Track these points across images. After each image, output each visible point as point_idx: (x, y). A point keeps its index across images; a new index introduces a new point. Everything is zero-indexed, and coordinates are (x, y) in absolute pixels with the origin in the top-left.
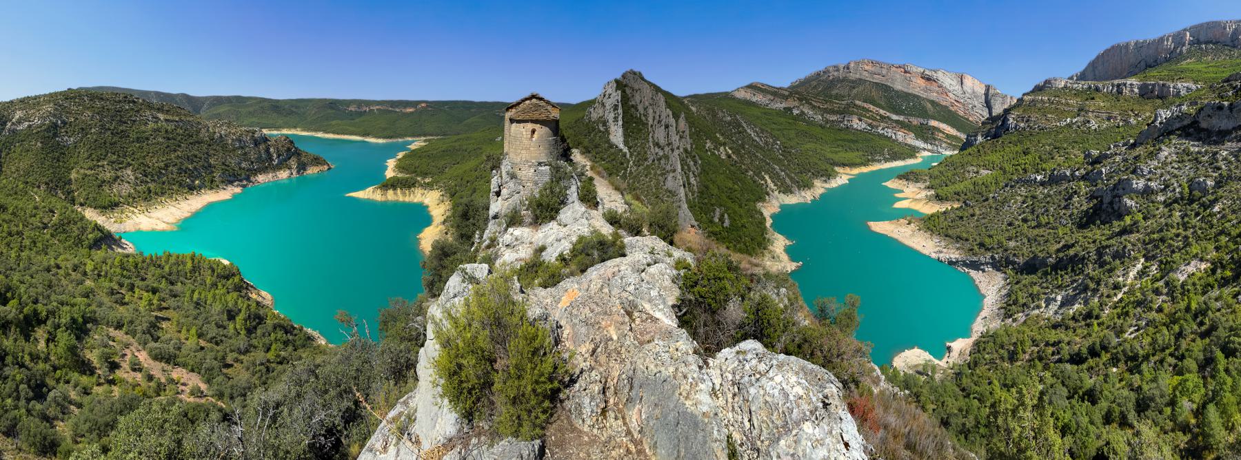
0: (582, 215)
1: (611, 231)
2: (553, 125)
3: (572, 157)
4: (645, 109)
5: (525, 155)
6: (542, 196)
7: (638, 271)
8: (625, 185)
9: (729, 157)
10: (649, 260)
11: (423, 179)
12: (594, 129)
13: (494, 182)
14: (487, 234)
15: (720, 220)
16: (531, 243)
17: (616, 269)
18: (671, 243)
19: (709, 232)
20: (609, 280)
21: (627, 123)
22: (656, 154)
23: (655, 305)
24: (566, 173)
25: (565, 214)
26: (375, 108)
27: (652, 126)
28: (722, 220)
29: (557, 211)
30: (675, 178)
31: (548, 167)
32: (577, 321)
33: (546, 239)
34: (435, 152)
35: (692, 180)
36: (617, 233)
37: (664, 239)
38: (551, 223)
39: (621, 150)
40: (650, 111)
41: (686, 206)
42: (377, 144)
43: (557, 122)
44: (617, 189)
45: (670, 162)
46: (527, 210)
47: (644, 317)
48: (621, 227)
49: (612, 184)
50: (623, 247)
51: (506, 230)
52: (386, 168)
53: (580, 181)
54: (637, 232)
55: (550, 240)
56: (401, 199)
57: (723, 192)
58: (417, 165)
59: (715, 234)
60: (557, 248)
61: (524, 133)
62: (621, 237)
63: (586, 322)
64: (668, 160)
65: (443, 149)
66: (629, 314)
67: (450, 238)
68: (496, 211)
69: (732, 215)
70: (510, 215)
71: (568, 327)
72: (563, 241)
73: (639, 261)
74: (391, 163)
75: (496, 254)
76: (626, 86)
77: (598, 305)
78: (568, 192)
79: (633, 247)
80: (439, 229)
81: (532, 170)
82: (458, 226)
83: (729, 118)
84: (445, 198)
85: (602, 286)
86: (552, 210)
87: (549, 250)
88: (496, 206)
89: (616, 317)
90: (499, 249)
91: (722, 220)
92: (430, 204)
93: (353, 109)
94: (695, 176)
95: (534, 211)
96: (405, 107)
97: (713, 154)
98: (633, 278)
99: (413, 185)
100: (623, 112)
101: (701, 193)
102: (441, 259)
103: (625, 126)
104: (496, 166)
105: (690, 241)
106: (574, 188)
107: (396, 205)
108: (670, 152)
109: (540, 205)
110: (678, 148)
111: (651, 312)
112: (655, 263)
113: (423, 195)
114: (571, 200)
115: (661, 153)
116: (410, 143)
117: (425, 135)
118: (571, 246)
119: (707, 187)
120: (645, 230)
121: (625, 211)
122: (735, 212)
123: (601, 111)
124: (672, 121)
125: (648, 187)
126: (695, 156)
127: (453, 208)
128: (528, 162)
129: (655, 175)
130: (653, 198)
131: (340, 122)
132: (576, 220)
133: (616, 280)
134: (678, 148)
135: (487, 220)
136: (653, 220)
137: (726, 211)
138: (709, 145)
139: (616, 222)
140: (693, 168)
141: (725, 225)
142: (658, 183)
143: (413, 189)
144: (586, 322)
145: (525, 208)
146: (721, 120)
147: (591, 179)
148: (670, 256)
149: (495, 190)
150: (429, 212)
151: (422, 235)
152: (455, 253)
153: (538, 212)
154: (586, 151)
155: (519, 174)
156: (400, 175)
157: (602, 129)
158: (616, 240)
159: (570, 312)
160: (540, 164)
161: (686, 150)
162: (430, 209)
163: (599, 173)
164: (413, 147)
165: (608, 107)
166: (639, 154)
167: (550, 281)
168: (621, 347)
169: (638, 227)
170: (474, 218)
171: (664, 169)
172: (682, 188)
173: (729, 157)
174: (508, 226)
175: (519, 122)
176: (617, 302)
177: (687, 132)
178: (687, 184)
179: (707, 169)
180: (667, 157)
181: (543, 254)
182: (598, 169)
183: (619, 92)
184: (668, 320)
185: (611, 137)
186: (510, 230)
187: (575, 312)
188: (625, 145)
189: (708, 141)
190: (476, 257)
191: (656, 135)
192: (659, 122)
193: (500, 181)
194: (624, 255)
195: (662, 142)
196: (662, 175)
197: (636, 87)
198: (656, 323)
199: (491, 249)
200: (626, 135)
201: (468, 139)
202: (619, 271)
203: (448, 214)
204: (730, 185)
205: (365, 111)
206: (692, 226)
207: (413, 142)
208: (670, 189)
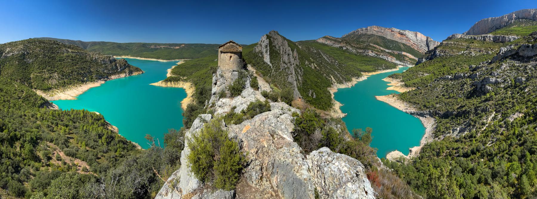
0: (252, 93)
1: (264, 100)
2: (239, 54)
4: (279, 47)
5: (227, 67)
6: (234, 85)
7: (276, 117)
8: (270, 80)
9: (316, 68)
10: (281, 112)
12: (257, 56)
13: (214, 79)
14: (211, 101)
15: (311, 95)
16: (230, 105)
18: (290, 105)
19: (307, 100)
20: (264, 121)
22: (284, 66)
23: (283, 132)
24: (245, 75)
25: (245, 93)
26: (162, 47)
27: (282, 54)
28: (312, 95)
29: (241, 91)
30: (292, 77)
31: (237, 72)
32: (249, 139)
34: (188, 66)
35: (300, 78)
37: (287, 103)
38: (238, 97)
39: (269, 65)
40: (281, 48)
41: (297, 89)
43: (241, 53)
44: (267, 82)
45: (290, 70)
46: (228, 91)
47: (279, 137)
48: (269, 98)
49: (265, 80)
50: (269, 107)
51: (219, 99)
52: (167, 73)
53: (251, 78)
54: (275, 100)
55: (238, 104)
56: (174, 86)
58: (180, 71)
59: (309, 101)
60: (241, 107)
61: (227, 58)
62: (269, 103)
63: (253, 139)
64: (289, 69)
65: (192, 64)
66: (272, 136)
67: (195, 103)
68: (215, 91)
69: (317, 93)
70: (220, 93)
71: (246, 142)
72: (243, 104)
74: (169, 71)
75: (215, 110)
76: (271, 37)
77: (259, 132)
78: (246, 83)
79: (274, 107)
80: (190, 99)
81: (230, 74)
83: (315, 51)
84: (193, 86)
86: (239, 91)
87: (238, 108)
88: (215, 89)
89: (266, 137)
90: (216, 108)
91: (312, 95)
92: (186, 88)
93: (153, 47)
94: (301, 76)
95: (231, 92)
96: (175, 46)
97: (309, 67)
98: (274, 120)
99: (179, 80)
100: (270, 49)
101: (303, 83)
102: (191, 112)
103: (271, 54)
104: (215, 72)
105: (299, 104)
106: (248, 81)
107: (172, 89)
108: (290, 66)
109: (233, 89)
110: (293, 64)
111: (282, 135)
112: (284, 114)
113: (183, 84)
114: (247, 86)
115: (286, 66)
116: (177, 62)
117: (184, 59)
119: (306, 81)
120: (279, 100)
121: (271, 91)
122: (318, 92)
124: (291, 52)
125: (280, 81)
126: (301, 68)
127: (196, 90)
128: (228, 70)
129: (283, 76)
131: (147, 53)
132: (249, 95)
133: (267, 121)
134: (293, 64)
135: (211, 95)
136: (282, 95)
137: (314, 91)
138: (307, 63)
139: (266, 96)
140: (300, 73)
141: (314, 97)
142: (285, 79)
143: (179, 82)
144: (253, 139)
145: (227, 90)
146: (312, 52)
147: (256, 77)
148: (290, 111)
149: (214, 82)
150: (186, 92)
151: (182, 102)
152: (197, 109)
153: (233, 92)
154: (253, 65)
155: (225, 75)
156: (173, 76)
157: (260, 56)
158: (267, 104)
159: (247, 135)
160: (234, 71)
161: (297, 65)
162: (186, 90)
163: (259, 75)
164: (179, 64)
165: (263, 46)
166: (276, 67)
167: (238, 122)
168: (269, 150)
170: (205, 94)
171: (287, 73)
173: (316, 68)
174: (220, 98)
175: (225, 53)
176: (267, 130)
177: (297, 57)
178: (297, 80)
179: (306, 73)
180: (288, 68)
181: (235, 110)
183: (268, 40)
184: (289, 139)
185: (264, 59)
186: (221, 99)
187: (249, 135)
188: (270, 63)
189: (306, 61)
190: (206, 111)
191: (284, 59)
192: (285, 53)
193: (216, 78)
194: (270, 110)
195: (287, 61)
196: (287, 76)
197: (275, 38)
199: (213, 108)
200: (271, 59)
202: (268, 117)
203: (194, 92)
204: (316, 80)
205: (158, 48)
206: (300, 98)
207: (179, 61)
208: (290, 82)
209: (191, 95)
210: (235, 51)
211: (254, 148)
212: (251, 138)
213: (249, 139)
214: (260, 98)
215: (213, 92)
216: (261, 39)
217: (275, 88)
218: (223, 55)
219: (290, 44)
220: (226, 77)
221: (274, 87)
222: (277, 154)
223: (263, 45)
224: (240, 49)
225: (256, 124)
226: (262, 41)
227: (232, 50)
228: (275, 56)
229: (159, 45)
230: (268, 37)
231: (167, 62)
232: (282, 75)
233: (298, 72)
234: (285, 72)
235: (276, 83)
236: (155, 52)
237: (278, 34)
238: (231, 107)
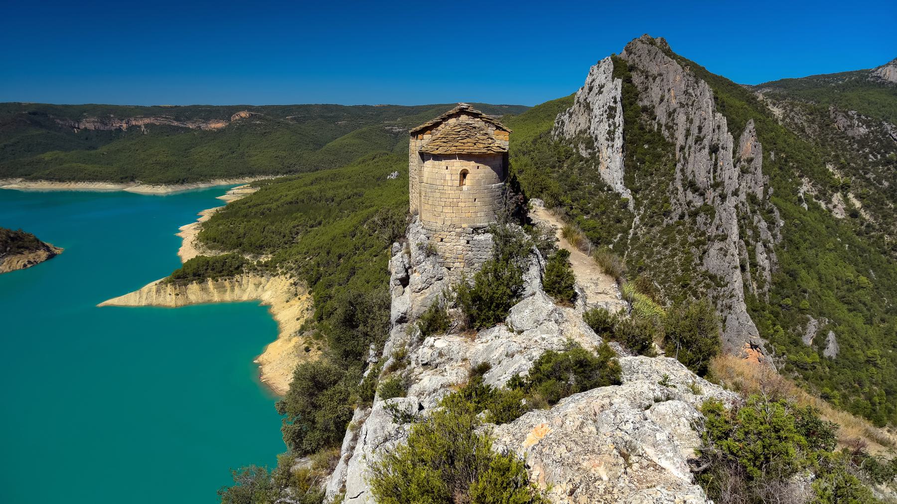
0: (549, 315)
1: (596, 344)
2: (499, 162)
3: (530, 215)
4: (670, 114)
5: (449, 215)
6: (480, 283)
7: (640, 407)
8: (622, 266)
9: (854, 214)
10: (658, 393)
11: (255, 257)
12: (569, 154)
13: (396, 265)
14: (389, 348)
15: (815, 342)
16: (464, 360)
17: (606, 401)
18: (703, 372)
19: (788, 362)
20: (595, 415)
21: (632, 142)
22: (689, 203)
23: (662, 451)
24: (521, 246)
25: (520, 314)
26: (140, 123)
27: (682, 148)
28: (820, 342)
29: (507, 308)
30: (724, 252)
31: (489, 236)
32: (549, 462)
33: (490, 353)
34: (274, 206)
35: (762, 258)
36: (606, 346)
37: (689, 364)
38: (497, 328)
39: (618, 195)
40: (681, 119)
41: (744, 307)
42: (154, 197)
43: (505, 156)
44: (609, 272)
45: (717, 221)
46: (455, 306)
47: (645, 463)
48: (613, 337)
49: (601, 263)
50: (617, 370)
51: (421, 340)
52: (179, 242)
53: (546, 258)
54: (642, 348)
55: (495, 355)
56: (216, 297)
57: (829, 288)
58: (242, 231)
59: (801, 367)
60: (508, 367)
61: (448, 177)
62: (613, 354)
63: (561, 462)
64: (713, 217)
65: (289, 199)
66: (626, 457)
67: (315, 356)
68: (403, 310)
69: (846, 336)
70: (427, 316)
71: (538, 468)
72: (517, 357)
73: (641, 393)
74: (189, 232)
75: (408, 377)
76: (632, 68)
77: (577, 443)
78: (524, 277)
79: (633, 371)
80: (293, 343)
81: (463, 241)
82: (338, 340)
83: (863, 130)
84: (300, 289)
85: (583, 423)
86: (498, 306)
87: (495, 370)
88: (399, 306)
89: (606, 457)
90: (412, 371)
91: (820, 342)
92: (273, 301)
93: (90, 126)
94: (768, 251)
95: (467, 309)
96: (207, 119)
97: (816, 208)
98: (632, 415)
99: (238, 270)
100: (626, 122)
101: (779, 285)
102: (311, 395)
103: (629, 149)
104: (399, 235)
105: (742, 374)
106: (534, 271)
107: (208, 310)
108: (718, 201)
109: (477, 298)
110: (735, 193)
111: (655, 459)
112: (668, 399)
113: (257, 285)
114: (529, 290)
115: (698, 202)
116: (223, 191)
117: (252, 174)
118: (530, 365)
119: (793, 275)
120: (656, 346)
121: (622, 312)
122: (854, 331)
123: (582, 120)
124: (727, 138)
125: (667, 266)
126: (771, 211)
127: (316, 306)
128: (454, 226)
129: (683, 244)
130: (676, 288)
131: (62, 155)
132: (538, 323)
133: (607, 415)
134: (735, 193)
135: (387, 326)
136: (671, 329)
137: (833, 326)
138: (806, 187)
139: (605, 330)
140: (765, 235)
141: (826, 353)
142: (688, 260)
143: (237, 277)
144: (561, 462)
145: (452, 304)
146: (843, 135)
147: (564, 254)
148: (696, 392)
149: (400, 276)
150: (272, 315)
151: (263, 358)
152: (335, 382)
153: (474, 310)
154: (554, 204)
155: (440, 247)
156: (209, 254)
157: (584, 154)
158: (607, 358)
159: (540, 449)
160: (476, 230)
161: (752, 198)
162: (274, 310)
163: (578, 244)
164: (229, 197)
165: (597, 112)
166: (652, 203)
167: (505, 415)
168: (613, 487)
169: (644, 340)
170: (365, 323)
171: (703, 233)
172: (738, 271)
173: (854, 214)
174: (425, 333)
175: (437, 157)
176: (609, 440)
177: (759, 161)
178: (749, 266)
179: (796, 237)
180: (710, 211)
181: (486, 376)
182: (576, 237)
183: (619, 82)
184: (684, 476)
185: (602, 169)
186: (429, 340)
187: (546, 451)
188: (626, 186)
189: (805, 180)
190: (373, 385)
191: (690, 167)
192: (699, 140)
193: (406, 261)
194: (619, 383)
195: (702, 179)
196: (698, 244)
197: (654, 70)
198: (661, 472)
199: (399, 372)
200: (630, 168)
201: (334, 178)
202: (611, 404)
203: (308, 315)
204: (849, 273)
205: (119, 129)
206: (754, 346)
207: (229, 188)
208: (712, 272)
209: (297, 326)
210: (480, 148)
211: (565, 483)
212: (553, 460)
213: (549, 462)
214: (581, 335)
215: (396, 312)
216: (589, 79)
217: (642, 298)
218: (434, 167)
219: (723, 96)
220: (447, 255)
221: (637, 295)
222: (638, 496)
223: (599, 104)
224: (501, 141)
225: (568, 422)
226: (591, 89)
227: (468, 147)
228: (647, 158)
229: (124, 113)
230: (622, 70)
231: (168, 198)
232: (674, 241)
233: (756, 230)
234: (692, 230)
235: (646, 274)
236: (103, 149)
237: (668, 53)
238: (469, 366)
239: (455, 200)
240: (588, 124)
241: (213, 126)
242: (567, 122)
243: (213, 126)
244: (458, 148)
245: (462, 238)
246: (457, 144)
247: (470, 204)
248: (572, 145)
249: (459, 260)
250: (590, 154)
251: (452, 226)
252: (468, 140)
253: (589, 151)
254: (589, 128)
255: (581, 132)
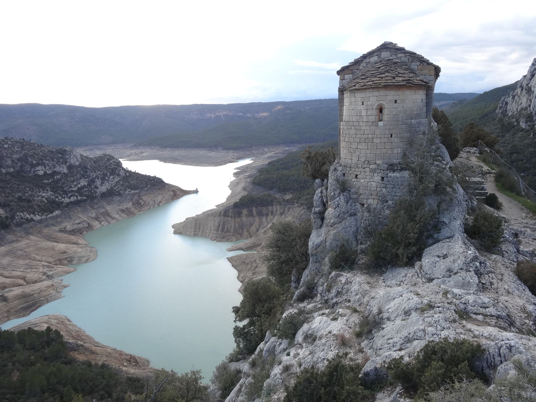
0: (467, 264)
61: (364, 113)
81: (377, 178)
157: (523, 125)
239: (370, 136)
240: (529, 103)
241: (261, 115)
242: (510, 103)
243: (261, 115)
244: (374, 82)
245: (376, 174)
246: (375, 79)
247: (386, 140)
248: (514, 120)
249: (373, 197)
250: (529, 126)
251: (366, 162)
252: (387, 74)
253: (529, 123)
254: (530, 106)
255: (522, 109)
